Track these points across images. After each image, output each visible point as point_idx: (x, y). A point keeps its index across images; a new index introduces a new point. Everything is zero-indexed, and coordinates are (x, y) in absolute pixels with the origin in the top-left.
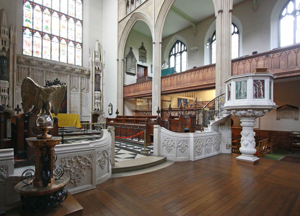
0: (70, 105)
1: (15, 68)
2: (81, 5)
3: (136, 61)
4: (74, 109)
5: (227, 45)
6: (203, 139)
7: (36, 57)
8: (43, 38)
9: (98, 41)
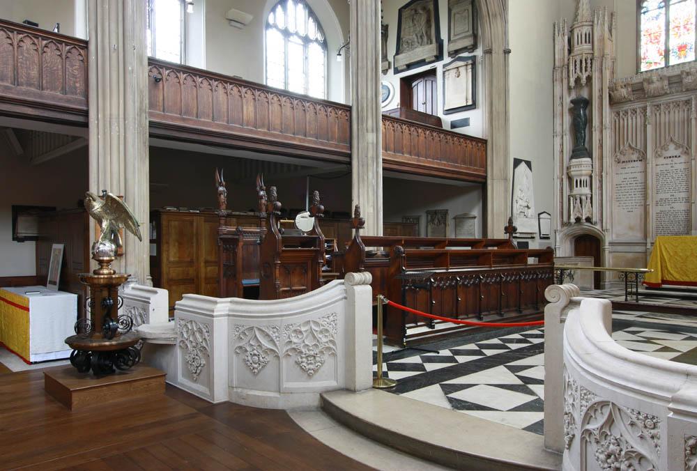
7: (679, 65)
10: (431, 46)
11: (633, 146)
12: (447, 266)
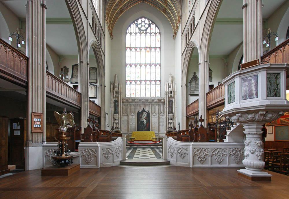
0: (152, 125)
1: (121, 106)
2: (160, 52)
5: (254, 41)
6: (203, 149)
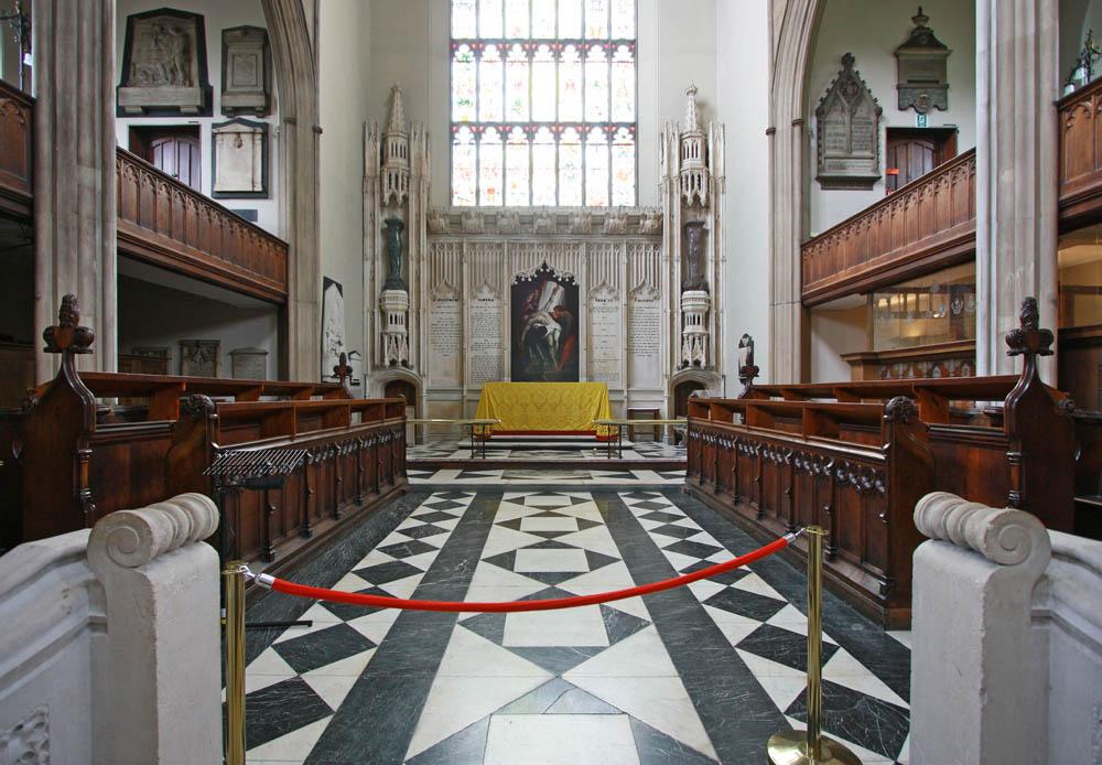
0: (589, 349)
3: (879, 112)
4: (604, 365)
8: (508, 142)
9: (695, 92)
10: (190, 89)
11: (450, 283)
12: (291, 433)
